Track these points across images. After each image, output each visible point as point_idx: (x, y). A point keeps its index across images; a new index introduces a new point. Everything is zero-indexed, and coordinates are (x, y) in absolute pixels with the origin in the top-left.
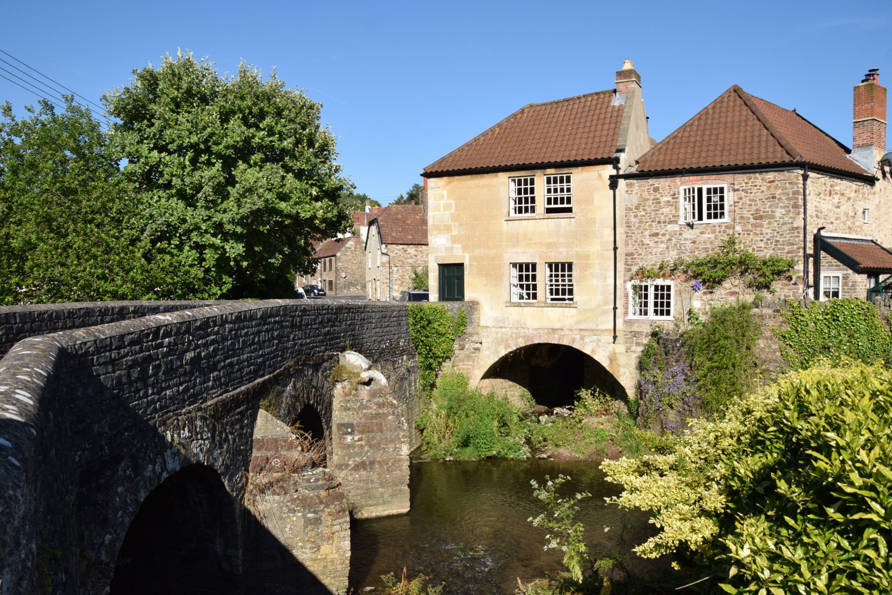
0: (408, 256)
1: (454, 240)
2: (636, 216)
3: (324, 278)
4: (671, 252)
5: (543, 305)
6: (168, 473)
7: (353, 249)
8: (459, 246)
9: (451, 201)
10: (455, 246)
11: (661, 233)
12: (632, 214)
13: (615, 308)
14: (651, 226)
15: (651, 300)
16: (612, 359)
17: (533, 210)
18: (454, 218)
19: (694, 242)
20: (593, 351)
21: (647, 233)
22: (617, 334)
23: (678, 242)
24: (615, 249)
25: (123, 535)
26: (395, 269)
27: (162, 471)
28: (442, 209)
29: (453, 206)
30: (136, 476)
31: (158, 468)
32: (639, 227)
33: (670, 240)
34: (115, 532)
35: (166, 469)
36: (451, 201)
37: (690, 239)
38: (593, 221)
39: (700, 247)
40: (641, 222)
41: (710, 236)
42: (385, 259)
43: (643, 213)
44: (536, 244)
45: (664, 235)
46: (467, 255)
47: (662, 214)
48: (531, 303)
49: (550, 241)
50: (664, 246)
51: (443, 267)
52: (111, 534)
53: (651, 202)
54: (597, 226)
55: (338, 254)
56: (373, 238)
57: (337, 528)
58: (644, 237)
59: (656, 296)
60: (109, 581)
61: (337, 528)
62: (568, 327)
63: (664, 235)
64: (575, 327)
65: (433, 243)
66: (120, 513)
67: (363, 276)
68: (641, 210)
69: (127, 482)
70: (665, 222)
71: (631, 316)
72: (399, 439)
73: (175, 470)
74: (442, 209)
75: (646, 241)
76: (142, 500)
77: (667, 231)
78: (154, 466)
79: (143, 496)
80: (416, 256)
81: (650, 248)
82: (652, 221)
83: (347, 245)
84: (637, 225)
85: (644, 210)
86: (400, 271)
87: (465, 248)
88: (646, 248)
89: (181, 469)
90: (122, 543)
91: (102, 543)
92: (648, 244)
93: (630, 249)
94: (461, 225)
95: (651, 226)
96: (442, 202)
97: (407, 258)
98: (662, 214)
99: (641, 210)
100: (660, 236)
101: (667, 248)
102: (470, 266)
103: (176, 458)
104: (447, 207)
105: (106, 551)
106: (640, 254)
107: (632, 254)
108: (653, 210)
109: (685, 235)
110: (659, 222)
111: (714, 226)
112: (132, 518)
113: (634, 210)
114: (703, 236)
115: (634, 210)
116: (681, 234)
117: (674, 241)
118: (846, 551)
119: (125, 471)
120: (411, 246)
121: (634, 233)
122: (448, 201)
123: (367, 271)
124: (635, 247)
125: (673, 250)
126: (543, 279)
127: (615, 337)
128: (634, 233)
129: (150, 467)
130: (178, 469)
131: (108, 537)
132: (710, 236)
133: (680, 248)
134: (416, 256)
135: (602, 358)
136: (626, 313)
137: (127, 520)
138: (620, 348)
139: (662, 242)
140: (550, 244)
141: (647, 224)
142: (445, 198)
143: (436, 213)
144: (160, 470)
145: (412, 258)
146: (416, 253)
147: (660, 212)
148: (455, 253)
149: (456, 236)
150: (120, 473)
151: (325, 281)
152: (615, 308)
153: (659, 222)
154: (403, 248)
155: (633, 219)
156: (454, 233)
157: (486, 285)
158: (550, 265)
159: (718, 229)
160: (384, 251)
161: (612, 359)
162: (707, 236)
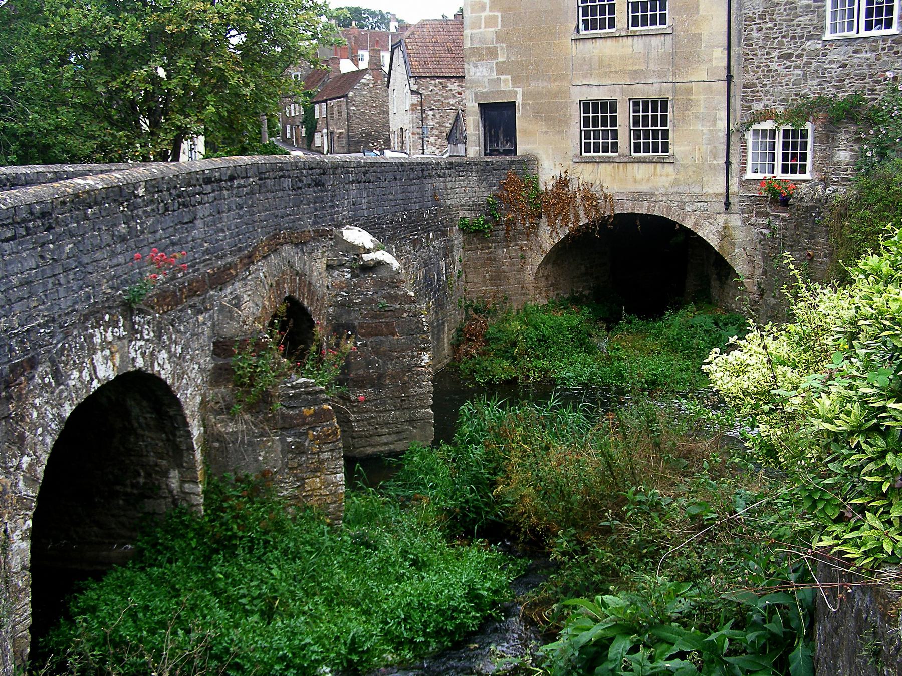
0: (449, 93)
1: (501, 69)
2: (760, 30)
3: (331, 129)
4: (809, 82)
5: (626, 160)
6: (99, 381)
7: (371, 85)
8: (509, 77)
9: (496, 13)
10: (502, 77)
11: (796, 53)
12: (754, 27)
13: (728, 163)
14: (781, 43)
15: (779, 151)
16: (725, 234)
17: (612, 24)
18: (499, 37)
19: (844, 66)
20: (696, 224)
21: (775, 54)
22: (731, 200)
23: (820, 66)
24: (729, 78)
25: (45, 458)
26: (431, 113)
27: (92, 379)
28: (483, 25)
29: (500, 19)
30: (58, 384)
31: (86, 376)
32: (763, 47)
33: (808, 63)
34: (35, 453)
35: (97, 377)
36: (496, 13)
37: (839, 61)
38: (698, 37)
39: (853, 72)
40: (766, 38)
41: (868, 55)
42: (416, 99)
43: (770, 25)
44: (616, 72)
45: (800, 56)
46: (519, 90)
47: (799, 25)
48: (609, 157)
49: (636, 68)
50: (799, 72)
51: (486, 108)
52: (28, 455)
53: (783, 7)
54: (703, 45)
55: (351, 94)
56: (399, 69)
57: (326, 455)
58: (771, 59)
59: (785, 145)
60: (30, 513)
61: (326, 455)
62: (663, 190)
63: (800, 56)
64: (672, 190)
65: (472, 73)
66: (40, 430)
67: (386, 124)
68: (767, 20)
69: (47, 392)
70: (801, 37)
71: (750, 175)
72: (417, 344)
73: (108, 378)
74: (483, 25)
75: (774, 66)
76: (68, 415)
77: (804, 49)
78: (81, 372)
79: (67, 410)
80: (460, 93)
81: (778, 75)
82: (783, 37)
83: (363, 81)
84: (761, 43)
85: (772, 20)
86: (438, 116)
87: (516, 80)
88: (773, 77)
89: (117, 377)
90: (44, 467)
91: (18, 467)
92: (777, 70)
93: (750, 77)
94: (510, 47)
95: (781, 43)
96: (483, 14)
97: (447, 98)
98: (799, 25)
99: (767, 20)
100: (793, 59)
101: (804, 75)
102: (524, 105)
103: (110, 363)
104: (490, 22)
105: (23, 476)
106: (765, 85)
107: (754, 85)
108: (785, 20)
109: (831, 56)
110: (793, 38)
111: (876, 41)
112: (56, 437)
113: (757, 21)
114: (858, 55)
115: (757, 21)
116: (825, 55)
117: (814, 64)
118: (865, 475)
119: (43, 378)
120: (453, 80)
121: (756, 55)
122: (491, 14)
123: (391, 115)
124: (757, 75)
125: (813, 79)
126: (628, 125)
127: (727, 204)
128: (756, 55)
129: (76, 374)
130: (112, 377)
131: (26, 459)
132: (868, 55)
133: (821, 75)
134: (460, 93)
135: (709, 234)
136: (743, 170)
137: (49, 440)
138: (735, 220)
139: (797, 67)
140: (636, 72)
141: (776, 41)
142: (488, 9)
143: (474, 31)
144: (88, 378)
145: (454, 96)
146: (460, 90)
147: (795, 22)
148: (503, 87)
149: (503, 62)
150: (38, 380)
151: (332, 133)
152: (728, 163)
153: (793, 38)
154: (441, 83)
155: (755, 34)
156: (500, 59)
157: (546, 132)
158: (636, 103)
159: (881, 44)
160: (415, 88)
161: (725, 234)
162: (864, 55)
